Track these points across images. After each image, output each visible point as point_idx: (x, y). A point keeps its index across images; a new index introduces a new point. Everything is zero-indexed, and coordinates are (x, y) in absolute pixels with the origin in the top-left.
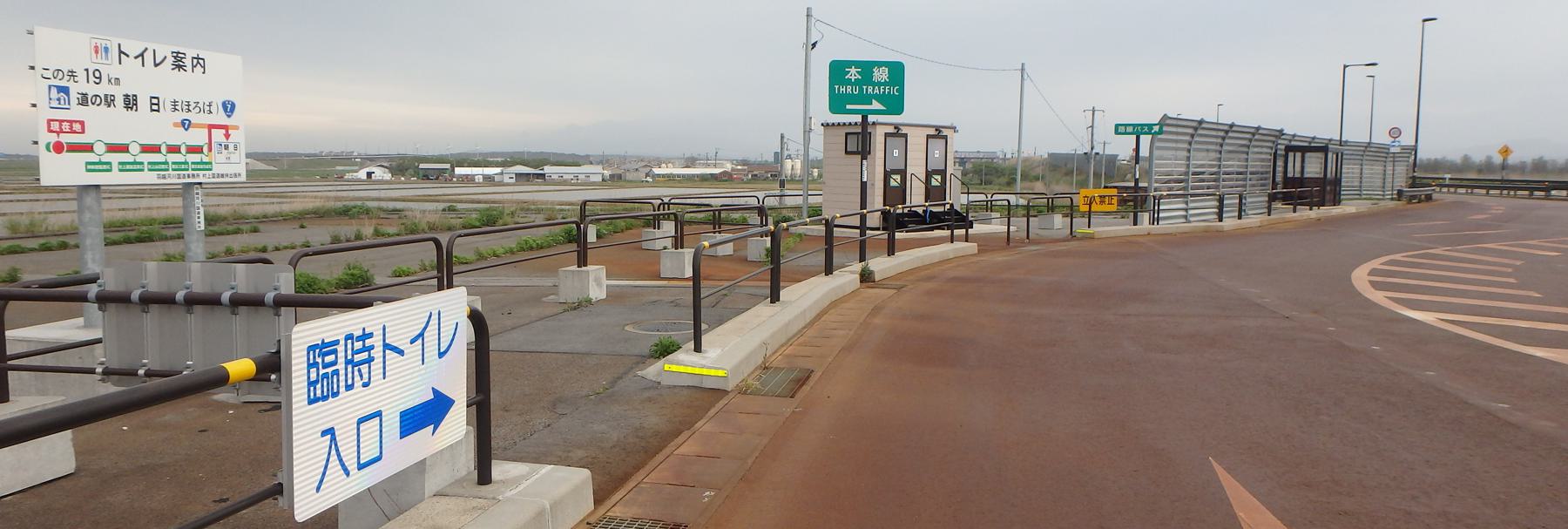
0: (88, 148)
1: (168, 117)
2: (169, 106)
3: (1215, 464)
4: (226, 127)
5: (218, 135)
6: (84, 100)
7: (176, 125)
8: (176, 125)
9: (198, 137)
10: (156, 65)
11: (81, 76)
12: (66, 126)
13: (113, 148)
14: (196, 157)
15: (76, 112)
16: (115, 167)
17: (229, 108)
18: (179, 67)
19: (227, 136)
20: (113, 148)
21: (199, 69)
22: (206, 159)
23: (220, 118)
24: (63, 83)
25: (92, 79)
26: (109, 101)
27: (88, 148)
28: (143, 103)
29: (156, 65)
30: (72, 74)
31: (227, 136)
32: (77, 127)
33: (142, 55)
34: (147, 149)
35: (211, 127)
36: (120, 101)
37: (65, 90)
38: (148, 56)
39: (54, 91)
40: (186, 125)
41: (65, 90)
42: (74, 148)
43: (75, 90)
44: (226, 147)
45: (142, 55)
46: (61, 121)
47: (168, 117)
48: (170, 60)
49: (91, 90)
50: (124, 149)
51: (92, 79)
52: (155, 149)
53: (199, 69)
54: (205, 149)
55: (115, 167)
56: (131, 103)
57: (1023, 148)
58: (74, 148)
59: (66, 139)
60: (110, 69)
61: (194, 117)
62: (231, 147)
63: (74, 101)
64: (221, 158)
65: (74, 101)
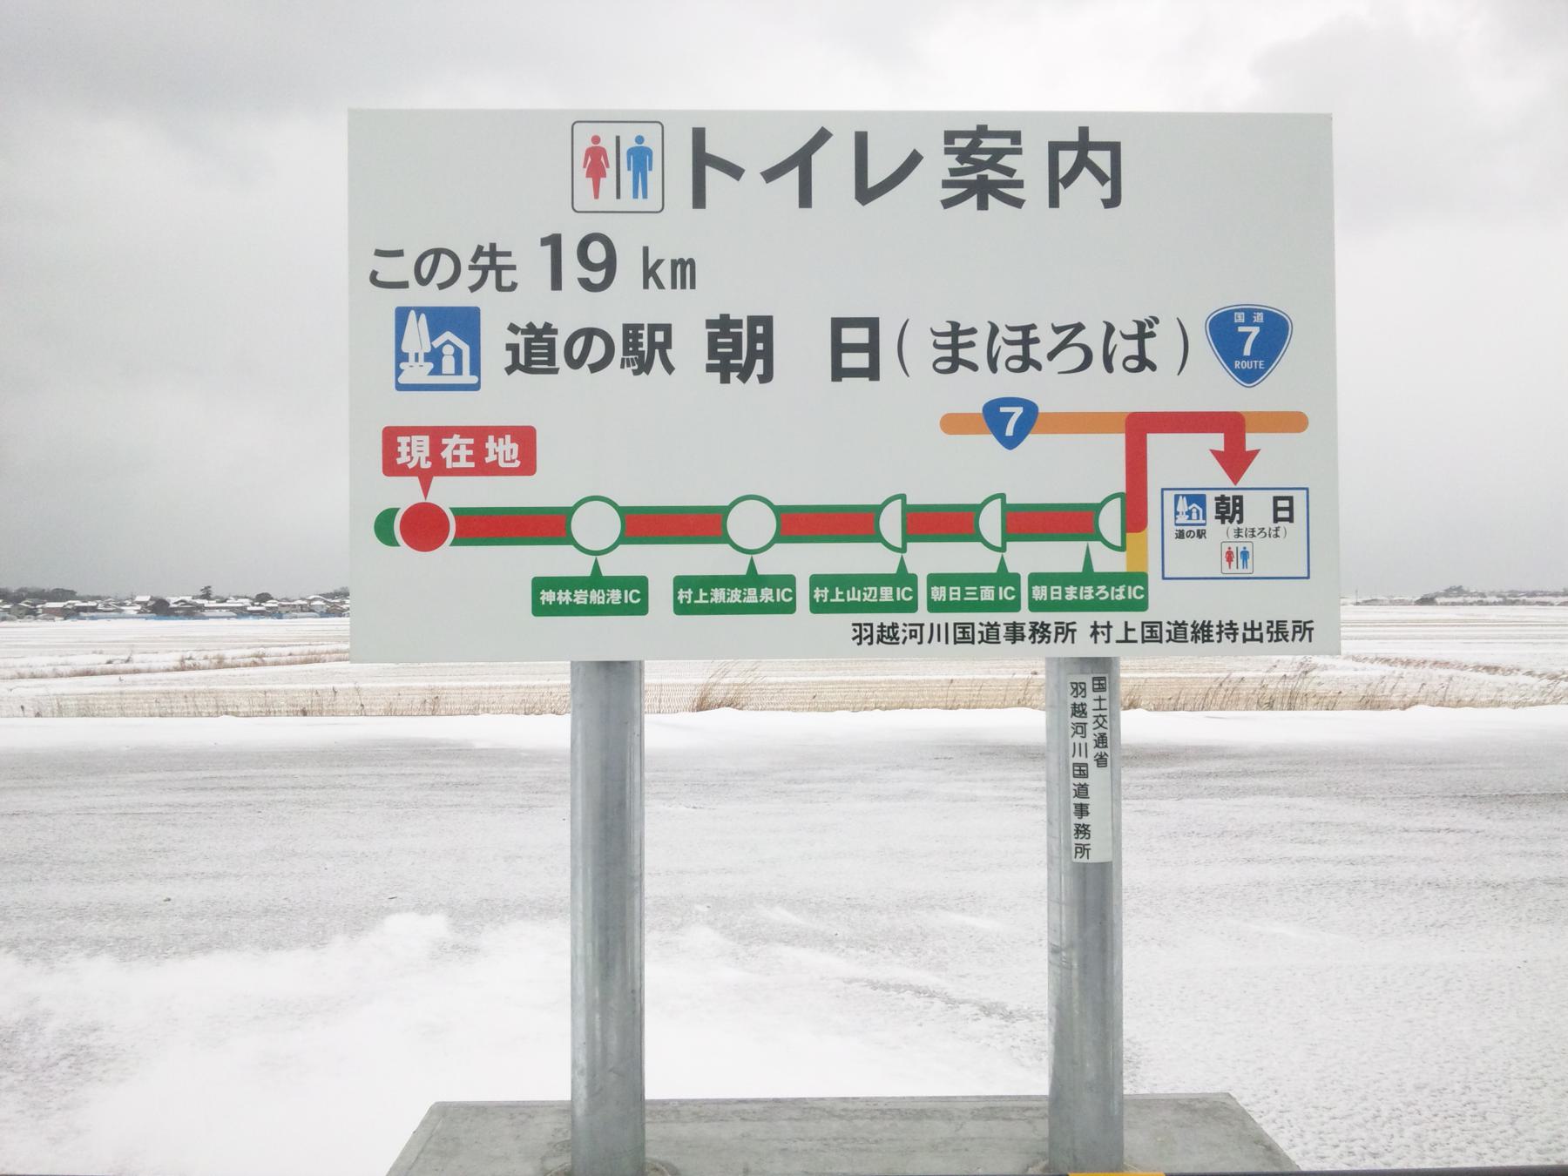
0: (549, 526)
1: (915, 392)
2: (922, 351)
3: (431, 98)
4: (1232, 426)
5: (1183, 462)
6: (536, 351)
7: (954, 424)
8: (954, 424)
9: (1083, 470)
10: (865, 194)
11: (531, 265)
12: (457, 450)
13: (644, 525)
14: (1063, 556)
15: (503, 397)
16: (661, 595)
17: (1252, 340)
18: (983, 191)
19: (1235, 460)
20: (644, 525)
21: (1087, 188)
22: (1107, 561)
23: (1210, 385)
24: (458, 297)
25: (572, 269)
26: (645, 348)
27: (549, 526)
28: (801, 348)
29: (865, 194)
30: (491, 261)
31: (1235, 460)
32: (503, 451)
33: (802, 161)
34: (798, 524)
35: (1139, 427)
36: (690, 347)
37: (465, 322)
38: (833, 167)
39: (417, 330)
40: (1009, 423)
41: (465, 322)
42: (485, 527)
43: (500, 320)
44: (1230, 509)
45: (802, 161)
46: (437, 435)
47: (915, 392)
48: (938, 164)
49: (568, 311)
50: (704, 525)
51: (572, 269)
52: (855, 523)
53: (1087, 188)
54: (1110, 521)
55: (661, 595)
56: (741, 348)
57: (1138, 1025)
58: (485, 527)
59: (451, 494)
60: (653, 225)
61: (1050, 388)
62: (1257, 510)
63: (495, 354)
64: (1204, 553)
65: (495, 354)
